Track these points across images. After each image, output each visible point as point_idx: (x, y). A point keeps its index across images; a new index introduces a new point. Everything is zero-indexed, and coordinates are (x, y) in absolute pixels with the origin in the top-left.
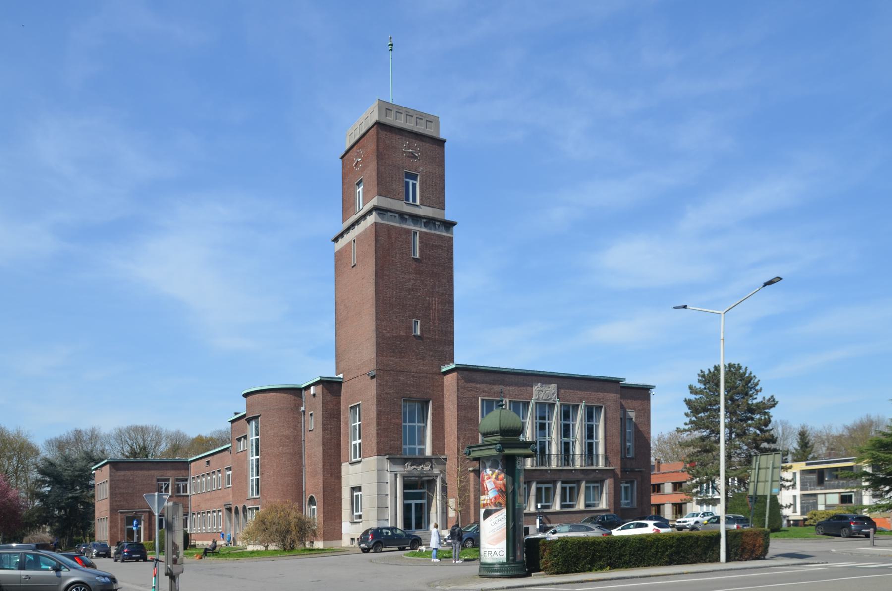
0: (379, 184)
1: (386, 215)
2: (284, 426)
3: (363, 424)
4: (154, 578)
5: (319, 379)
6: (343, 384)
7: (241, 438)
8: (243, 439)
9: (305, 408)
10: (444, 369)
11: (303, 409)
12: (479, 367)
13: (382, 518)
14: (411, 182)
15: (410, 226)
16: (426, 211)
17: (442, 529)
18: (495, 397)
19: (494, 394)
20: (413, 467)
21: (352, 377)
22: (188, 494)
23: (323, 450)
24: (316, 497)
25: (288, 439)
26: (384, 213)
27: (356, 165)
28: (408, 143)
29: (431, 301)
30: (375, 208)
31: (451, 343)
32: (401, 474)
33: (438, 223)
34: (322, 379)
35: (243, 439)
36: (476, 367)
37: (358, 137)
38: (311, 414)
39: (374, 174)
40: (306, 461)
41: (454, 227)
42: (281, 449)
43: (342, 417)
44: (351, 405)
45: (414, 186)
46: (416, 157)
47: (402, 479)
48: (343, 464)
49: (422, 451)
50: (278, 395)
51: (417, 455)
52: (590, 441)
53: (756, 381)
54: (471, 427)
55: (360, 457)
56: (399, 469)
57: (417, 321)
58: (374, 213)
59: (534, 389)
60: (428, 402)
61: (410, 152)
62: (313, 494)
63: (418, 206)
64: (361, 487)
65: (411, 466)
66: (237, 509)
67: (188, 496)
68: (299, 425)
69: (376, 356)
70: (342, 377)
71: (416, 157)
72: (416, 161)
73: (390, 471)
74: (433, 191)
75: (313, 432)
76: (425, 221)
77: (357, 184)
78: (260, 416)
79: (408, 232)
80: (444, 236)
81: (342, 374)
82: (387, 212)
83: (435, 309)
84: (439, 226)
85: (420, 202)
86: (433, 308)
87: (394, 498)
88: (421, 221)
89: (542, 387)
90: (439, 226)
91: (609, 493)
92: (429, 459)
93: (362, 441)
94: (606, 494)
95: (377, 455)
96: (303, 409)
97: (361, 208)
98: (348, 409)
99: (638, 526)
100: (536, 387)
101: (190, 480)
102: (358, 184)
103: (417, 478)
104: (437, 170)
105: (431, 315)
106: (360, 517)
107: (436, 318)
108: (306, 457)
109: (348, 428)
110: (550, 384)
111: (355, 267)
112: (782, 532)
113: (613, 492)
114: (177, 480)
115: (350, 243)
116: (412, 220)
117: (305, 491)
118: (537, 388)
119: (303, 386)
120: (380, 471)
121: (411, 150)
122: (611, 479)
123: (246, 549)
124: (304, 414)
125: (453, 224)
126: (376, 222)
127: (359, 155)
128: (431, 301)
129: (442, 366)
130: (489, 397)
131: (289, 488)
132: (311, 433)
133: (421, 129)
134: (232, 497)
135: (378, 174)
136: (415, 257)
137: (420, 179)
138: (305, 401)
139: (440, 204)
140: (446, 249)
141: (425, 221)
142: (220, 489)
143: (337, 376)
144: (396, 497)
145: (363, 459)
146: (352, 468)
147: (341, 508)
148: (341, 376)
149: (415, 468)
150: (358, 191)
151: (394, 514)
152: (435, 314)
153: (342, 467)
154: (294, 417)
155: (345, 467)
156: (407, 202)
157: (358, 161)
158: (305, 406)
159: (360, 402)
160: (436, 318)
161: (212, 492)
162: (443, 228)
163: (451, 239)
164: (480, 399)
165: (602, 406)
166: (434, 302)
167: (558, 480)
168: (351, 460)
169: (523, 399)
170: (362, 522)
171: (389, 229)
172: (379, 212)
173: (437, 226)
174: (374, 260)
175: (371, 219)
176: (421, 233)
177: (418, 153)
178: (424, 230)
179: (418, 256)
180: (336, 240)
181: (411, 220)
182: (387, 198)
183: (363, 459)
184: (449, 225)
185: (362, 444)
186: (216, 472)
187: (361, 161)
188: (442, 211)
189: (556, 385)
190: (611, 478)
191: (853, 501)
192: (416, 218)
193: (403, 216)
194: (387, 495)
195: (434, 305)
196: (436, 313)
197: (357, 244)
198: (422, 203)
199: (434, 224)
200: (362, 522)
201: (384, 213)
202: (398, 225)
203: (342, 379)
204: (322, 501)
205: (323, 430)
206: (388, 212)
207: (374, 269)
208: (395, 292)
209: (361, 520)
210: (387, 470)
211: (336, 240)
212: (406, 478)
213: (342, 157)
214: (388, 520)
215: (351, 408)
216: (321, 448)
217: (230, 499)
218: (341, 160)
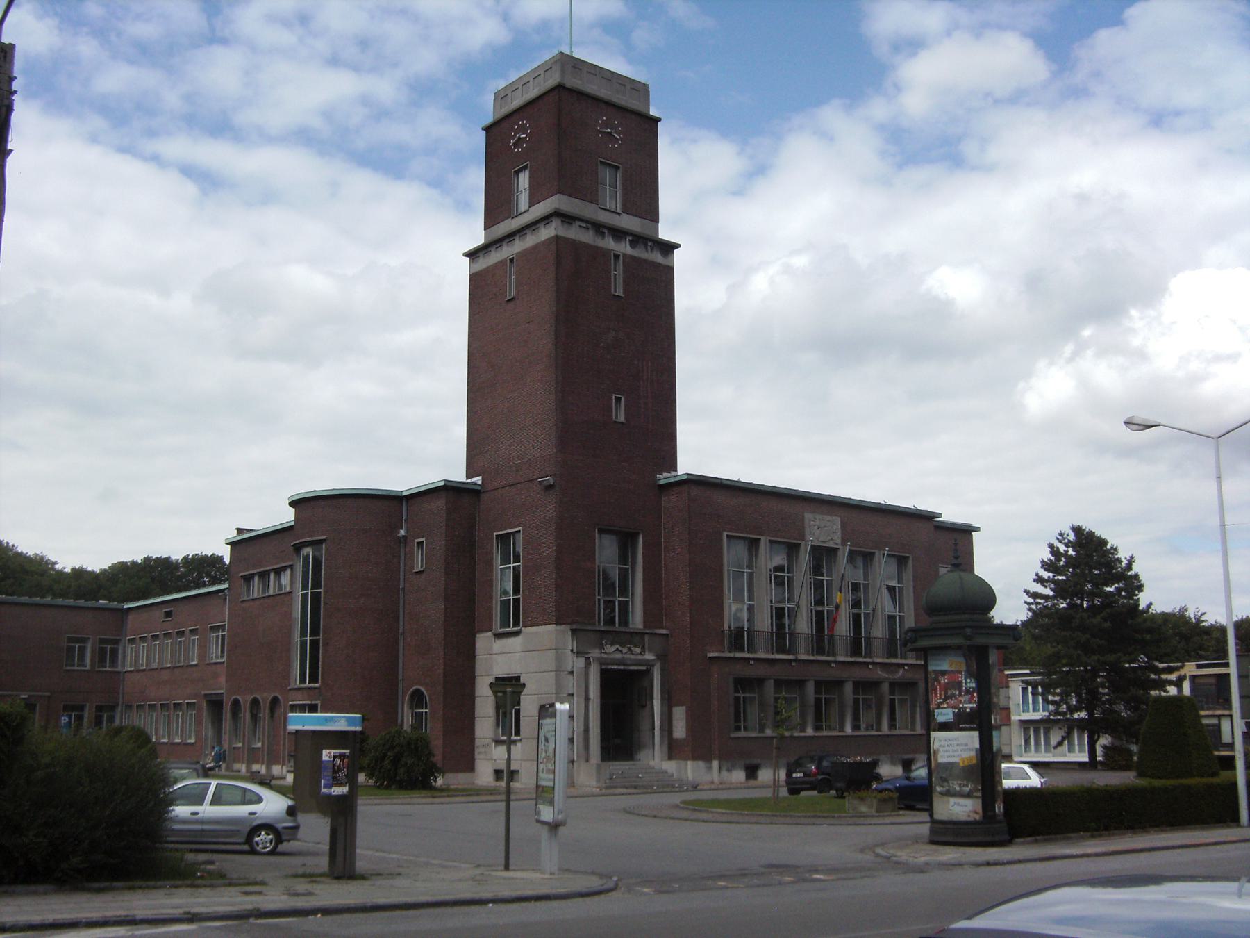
1: (574, 225)
3: (525, 567)
4: (803, 794)
5: (443, 483)
6: (482, 495)
7: (254, 574)
8: (256, 579)
9: (407, 531)
11: (402, 532)
15: (609, 243)
16: (629, 222)
17: (662, 760)
22: (119, 669)
23: (446, 608)
24: (427, 690)
27: (515, 144)
30: (557, 214)
34: (449, 484)
35: (256, 579)
38: (420, 544)
41: (675, 251)
44: (498, 533)
52: (820, 608)
56: (595, 653)
60: (638, 534)
62: (421, 685)
64: (519, 677)
66: (236, 703)
67: (119, 673)
70: (480, 483)
73: (577, 653)
75: (423, 576)
76: (631, 238)
78: (325, 540)
79: (605, 253)
81: (480, 478)
82: (575, 221)
84: (652, 250)
86: (645, 378)
90: (652, 250)
95: (556, 624)
96: (402, 532)
101: (125, 643)
111: (513, 302)
114: (102, 641)
119: (404, 494)
121: (609, 130)
123: (285, 778)
124: (405, 543)
134: (227, 681)
139: (652, 214)
141: (631, 238)
142: (196, 665)
143: (469, 481)
144: (587, 699)
146: (498, 645)
147: (473, 712)
148: (478, 480)
155: (483, 641)
157: (520, 138)
161: (175, 670)
163: (670, 270)
164: (725, 534)
167: (847, 681)
170: (520, 740)
171: (575, 245)
172: (564, 220)
173: (649, 248)
175: (546, 233)
179: (620, 292)
186: (187, 632)
187: (526, 138)
192: (618, 234)
193: (598, 228)
194: (573, 695)
199: (646, 246)
200: (520, 740)
204: (442, 699)
208: (586, 349)
209: (519, 738)
212: (603, 667)
217: (220, 686)
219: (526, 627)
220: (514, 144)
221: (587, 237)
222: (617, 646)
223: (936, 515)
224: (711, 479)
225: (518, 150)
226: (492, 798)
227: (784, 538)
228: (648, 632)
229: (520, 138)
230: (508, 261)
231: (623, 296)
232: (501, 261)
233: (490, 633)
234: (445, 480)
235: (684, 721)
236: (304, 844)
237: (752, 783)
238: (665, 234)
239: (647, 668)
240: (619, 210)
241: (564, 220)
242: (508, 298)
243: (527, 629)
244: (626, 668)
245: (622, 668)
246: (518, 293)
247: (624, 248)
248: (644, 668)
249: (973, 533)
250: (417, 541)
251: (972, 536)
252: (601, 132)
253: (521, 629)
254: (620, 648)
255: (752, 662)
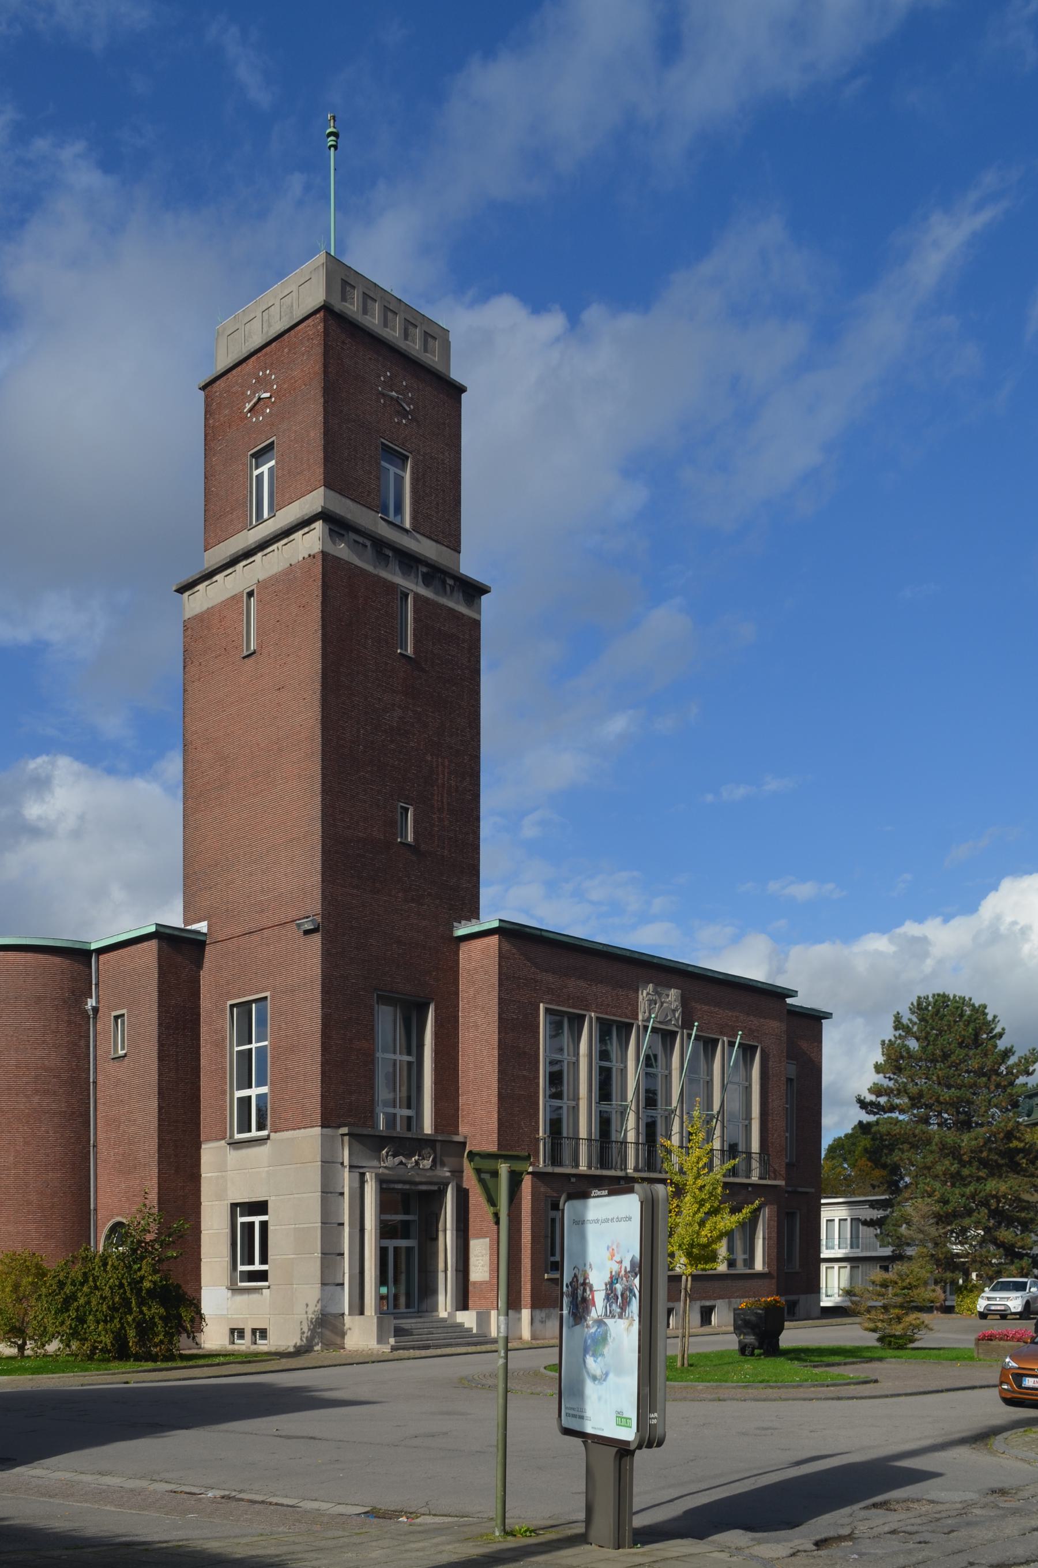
0: (328, 459)
2: (44, 1042)
5: (153, 929)
6: (207, 948)
9: (98, 1002)
10: (460, 932)
12: (544, 933)
13: (330, 1281)
14: (393, 470)
17: (457, 1310)
18: (570, 1007)
19: (568, 1000)
20: (397, 1160)
21: (238, 931)
23: (160, 1108)
25: (55, 1077)
26: (342, 532)
28: (388, 374)
29: (434, 766)
31: (473, 871)
32: (377, 1175)
33: (450, 582)
34: (162, 930)
36: (539, 933)
37: (257, 341)
39: (316, 435)
40: (102, 1134)
42: (36, 1099)
43: (204, 1029)
45: (399, 480)
46: (404, 414)
47: (379, 1187)
48: (203, 1146)
49: (413, 1122)
50: (57, 960)
51: (400, 1129)
53: (998, 1030)
54: (525, 1073)
55: (261, 1127)
57: (407, 810)
58: (318, 525)
59: (641, 997)
61: (392, 398)
63: (406, 531)
64: (267, 1201)
65: (394, 1156)
68: (82, 1043)
69: (323, 881)
70: (205, 930)
71: (404, 414)
72: (404, 421)
73: (351, 1167)
74: (438, 504)
76: (425, 570)
77: (253, 456)
79: (392, 587)
80: (463, 615)
83: (443, 785)
84: (452, 591)
85: (412, 523)
87: (357, 1230)
88: (418, 570)
89: (656, 992)
90: (452, 591)
91: (769, 1238)
92: (428, 1143)
93: (272, 1090)
94: (764, 1239)
96: (91, 1002)
97: (266, 515)
98: (223, 1010)
99: (999, 1287)
100: (645, 992)
102: (260, 456)
103: (407, 1187)
104: (447, 454)
105: (436, 797)
106: (263, 1276)
107: (446, 807)
108: (99, 1125)
109: (224, 1056)
110: (670, 987)
111: (253, 657)
112: (907, 1351)
113: (774, 1235)
115: (235, 599)
116: (400, 562)
117: (95, 1210)
118: (648, 994)
119: (93, 947)
120: (328, 1165)
122: (772, 1207)
125: (483, 590)
126: (326, 550)
127: (263, 383)
128: (434, 766)
129: (455, 924)
130: (559, 1005)
131: (56, 1200)
132: (116, 1063)
133: (415, 347)
135: (326, 433)
136: (404, 652)
137: (412, 467)
138: (97, 985)
139: (453, 541)
140: (465, 645)
141: (425, 570)
145: (272, 1134)
146: (234, 1156)
148: (202, 927)
149: (401, 1163)
150: (256, 473)
151: (357, 1271)
152: (442, 797)
153: (202, 1151)
154: (69, 1022)
155: (211, 1154)
156: (386, 517)
157: (260, 399)
158: (98, 997)
159: (267, 994)
160: (446, 807)
162: (461, 595)
163: (476, 624)
165: (757, 1047)
166: (440, 768)
168: (232, 1136)
169: (620, 1016)
174: (320, 644)
176: (417, 597)
177: (409, 405)
178: (423, 591)
180: (254, 561)
181: (397, 562)
182: (344, 499)
183: (272, 1134)
184: (474, 591)
185: (272, 1098)
188: (456, 554)
189: (680, 991)
190: (771, 1204)
191: (713, 1323)
192: (409, 561)
195: (441, 776)
196: (445, 795)
197: (260, 601)
198: (416, 527)
201: (342, 532)
202: (370, 568)
203: (205, 934)
205: (161, 1059)
206: (351, 534)
207: (320, 666)
210: (342, 1164)
211: (254, 561)
212: (384, 1186)
213: (204, 388)
214: (343, 1284)
215: (232, 1006)
216: (155, 1104)
218: (202, 393)
219: (275, 1132)
220: (250, 411)
221: (364, 563)
222: (401, 1158)
223: (791, 993)
224: (528, 930)
225: (257, 419)
226: (424, 1353)
227: (614, 1015)
228: (439, 1138)
229: (260, 399)
230: (245, 595)
231: (413, 656)
232: (233, 598)
233: (224, 1141)
234: (157, 924)
235: (487, 1258)
236: (471, 1519)
237: (706, 1329)
238: (469, 566)
239: (439, 1188)
240: (407, 525)
241: (332, 528)
242: (245, 653)
243: (278, 1134)
244: (413, 1187)
245: (407, 1187)
246: (260, 645)
247: (414, 586)
248: (435, 1188)
249: (822, 1021)
250: (115, 1013)
251: (822, 1023)
252: (383, 395)
253: (269, 1136)
254: (404, 1160)
255: (573, 1180)
